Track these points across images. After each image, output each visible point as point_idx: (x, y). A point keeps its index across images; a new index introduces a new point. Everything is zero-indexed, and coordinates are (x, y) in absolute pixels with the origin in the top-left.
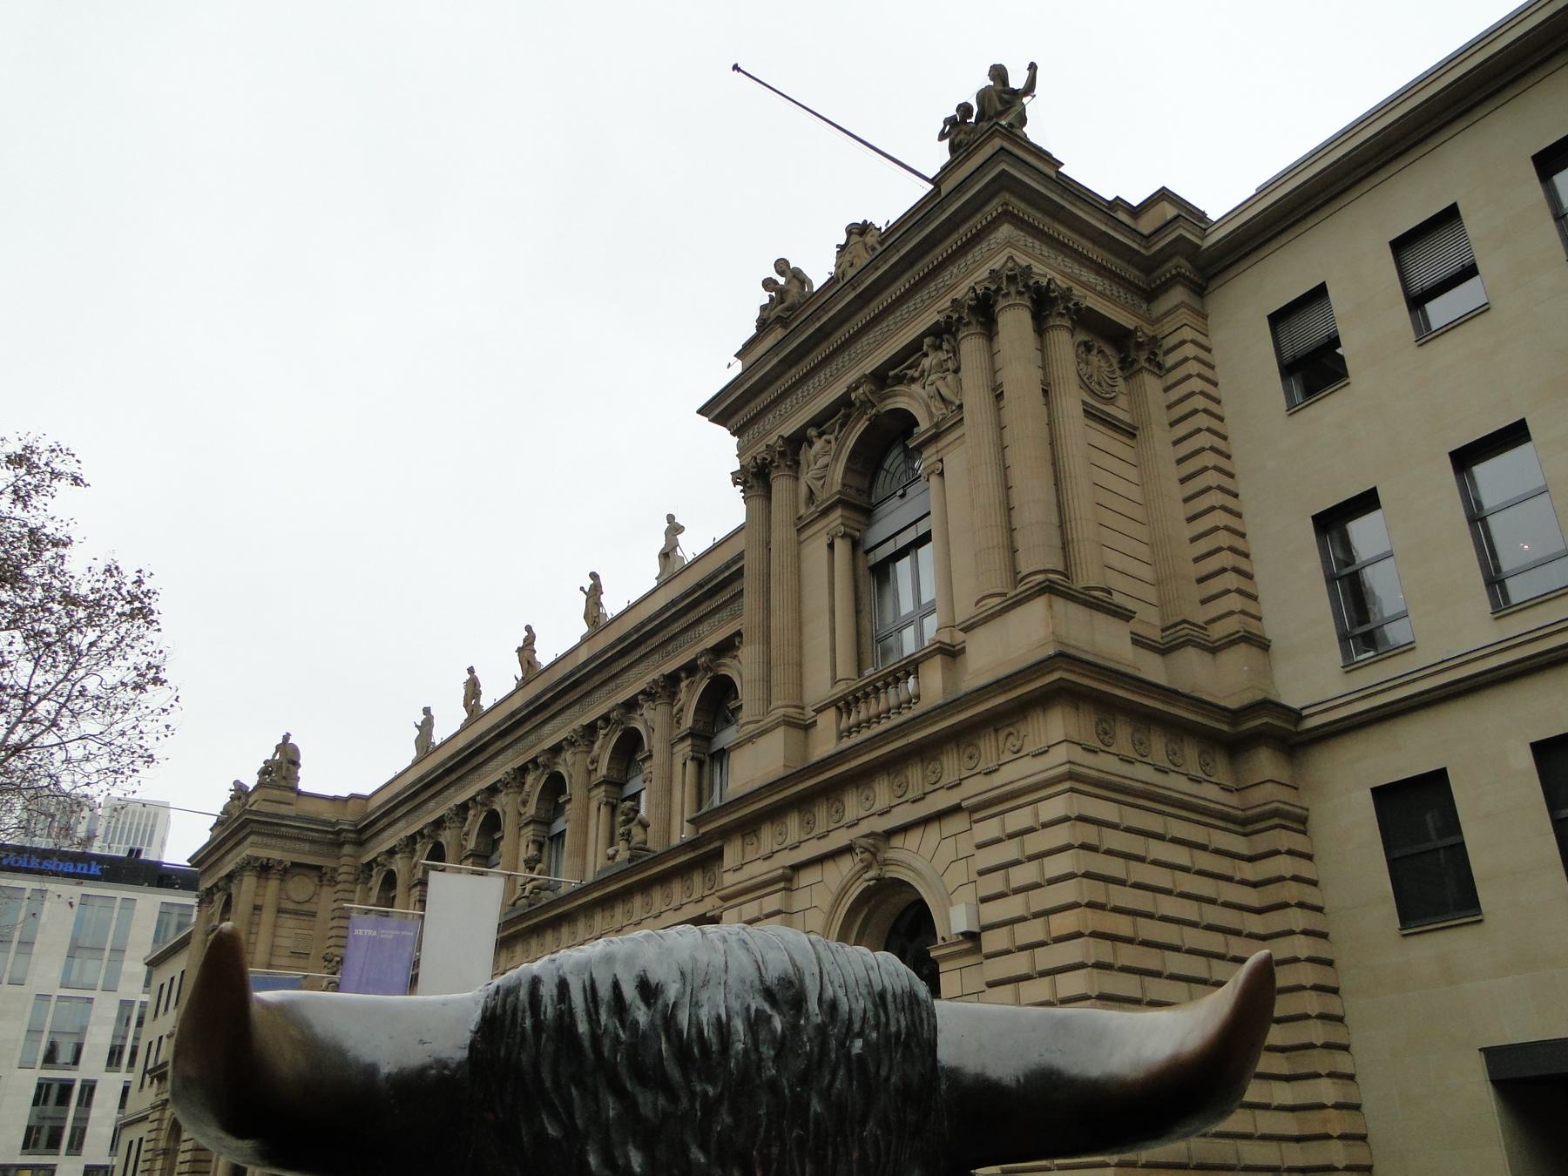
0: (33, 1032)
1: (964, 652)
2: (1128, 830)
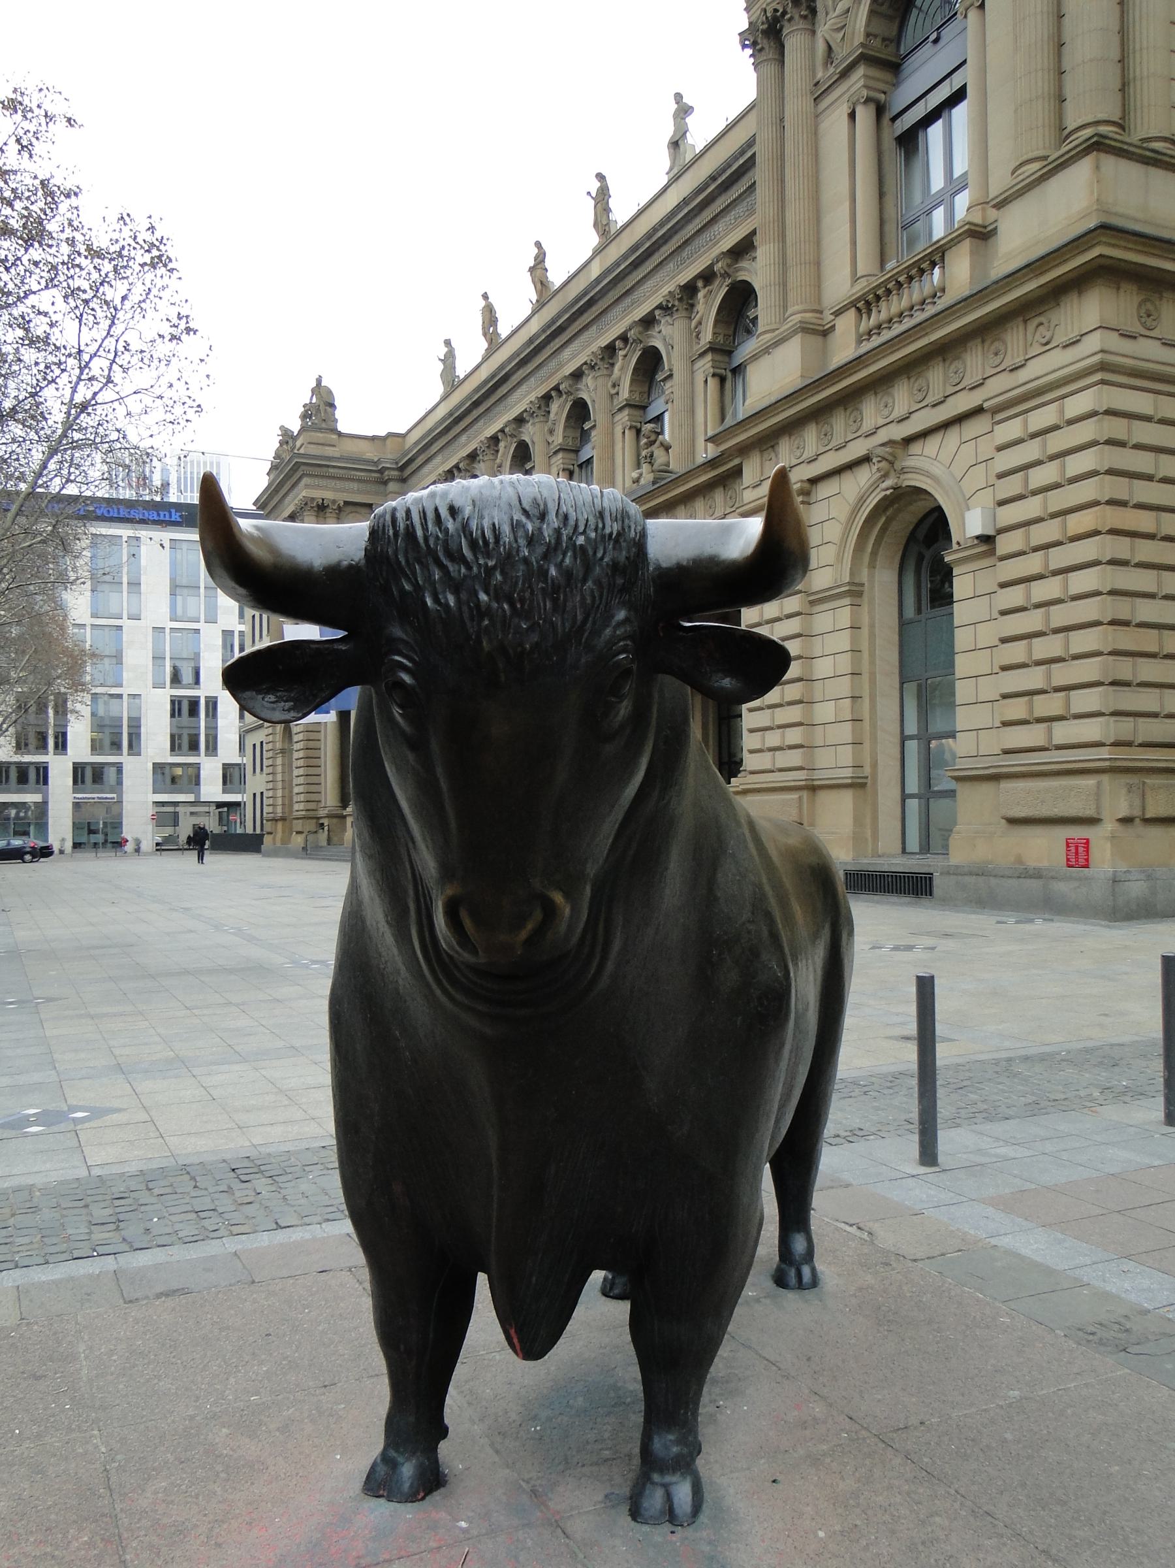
0: (158, 658)
1: (996, 233)
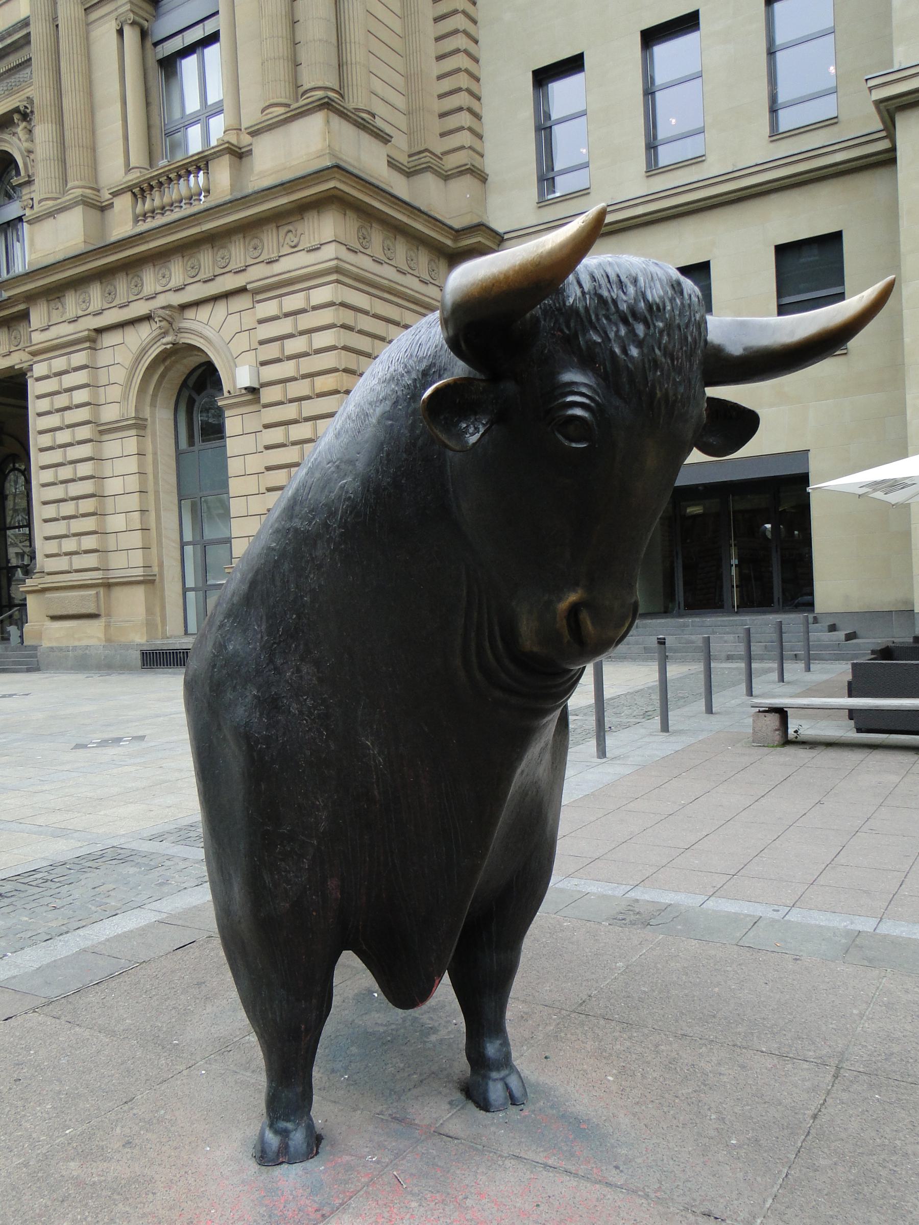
2: (375, 316)
